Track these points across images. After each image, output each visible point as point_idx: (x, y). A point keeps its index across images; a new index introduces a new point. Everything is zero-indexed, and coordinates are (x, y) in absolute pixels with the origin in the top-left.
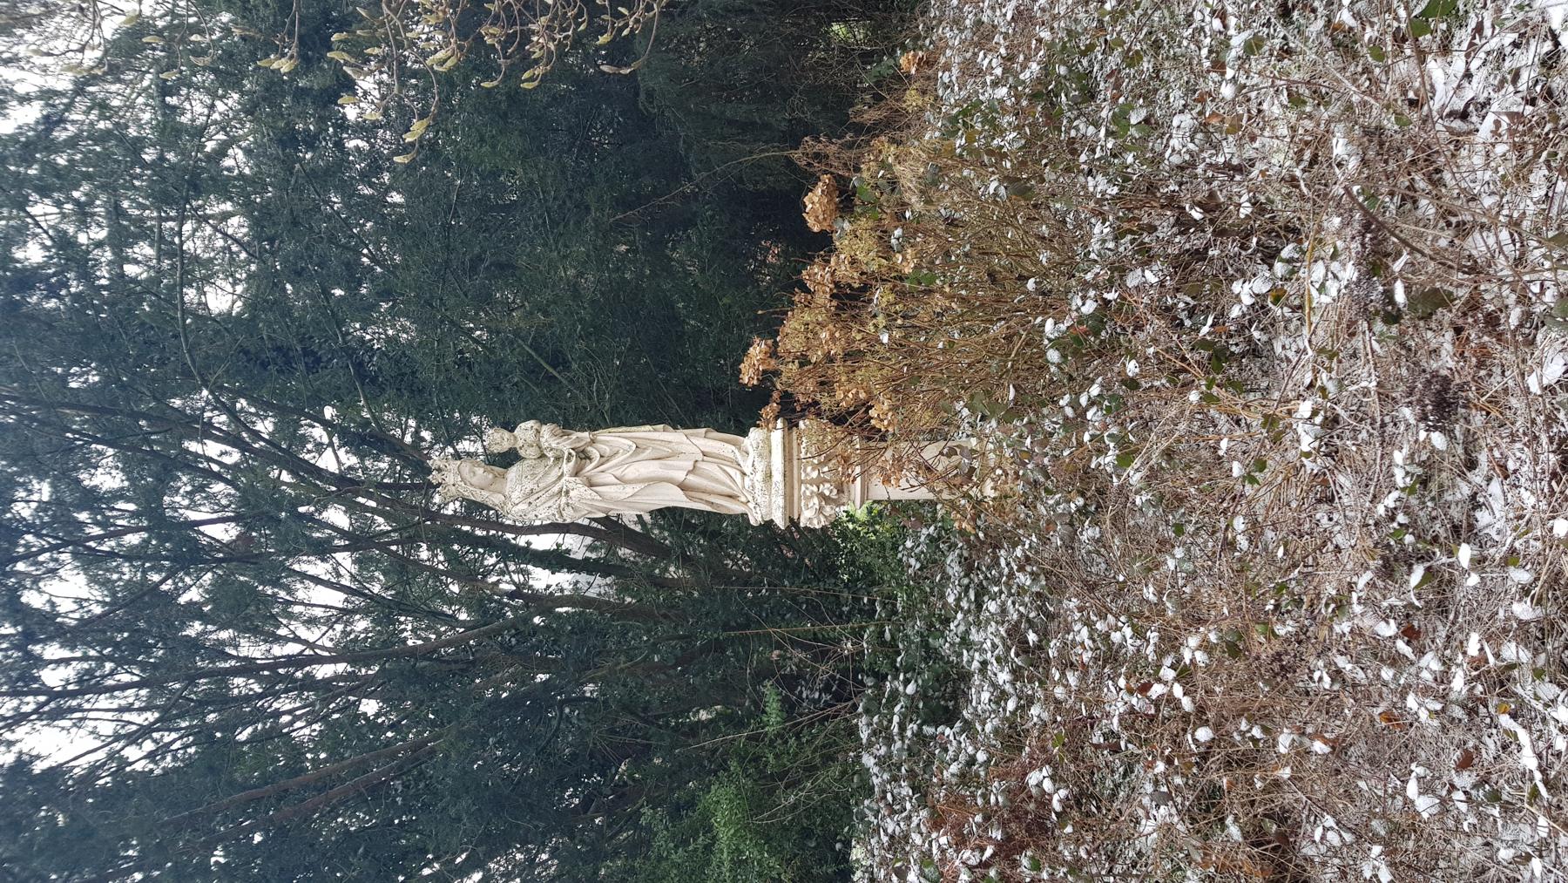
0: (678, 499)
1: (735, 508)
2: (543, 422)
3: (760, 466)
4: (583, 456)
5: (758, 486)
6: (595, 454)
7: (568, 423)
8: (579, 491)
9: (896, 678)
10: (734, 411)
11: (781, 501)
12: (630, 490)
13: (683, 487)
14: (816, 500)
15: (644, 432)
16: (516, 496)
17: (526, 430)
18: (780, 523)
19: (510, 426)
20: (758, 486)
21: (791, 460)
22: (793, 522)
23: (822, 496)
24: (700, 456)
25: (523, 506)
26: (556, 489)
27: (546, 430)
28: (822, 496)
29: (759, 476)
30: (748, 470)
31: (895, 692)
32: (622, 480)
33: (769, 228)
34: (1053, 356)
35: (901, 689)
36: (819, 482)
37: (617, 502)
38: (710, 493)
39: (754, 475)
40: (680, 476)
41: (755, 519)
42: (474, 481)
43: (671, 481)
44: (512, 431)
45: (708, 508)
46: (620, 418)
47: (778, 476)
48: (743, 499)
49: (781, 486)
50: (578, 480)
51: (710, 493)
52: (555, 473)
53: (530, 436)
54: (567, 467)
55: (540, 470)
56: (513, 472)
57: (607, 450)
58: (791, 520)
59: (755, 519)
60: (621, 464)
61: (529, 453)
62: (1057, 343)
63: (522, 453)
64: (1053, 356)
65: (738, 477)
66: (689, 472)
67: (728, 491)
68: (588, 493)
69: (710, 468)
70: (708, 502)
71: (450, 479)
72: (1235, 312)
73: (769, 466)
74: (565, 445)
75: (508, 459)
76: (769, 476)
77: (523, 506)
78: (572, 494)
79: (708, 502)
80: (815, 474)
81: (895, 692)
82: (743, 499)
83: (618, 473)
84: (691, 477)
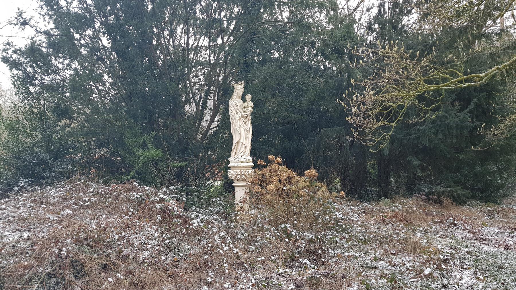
0: (235, 141)
1: (233, 154)
2: (253, 108)
3: (244, 160)
4: (246, 118)
5: (239, 160)
6: (246, 120)
7: (252, 114)
8: (238, 117)
10: (257, 153)
11: (236, 165)
12: (238, 129)
13: (239, 141)
15: (251, 132)
16: (236, 102)
17: (251, 104)
18: (229, 165)
19: (252, 100)
20: (239, 160)
22: (229, 168)
23: (237, 175)
27: (251, 109)
28: (237, 175)
29: (242, 160)
30: (243, 157)
31: (182, 195)
33: (295, 162)
34: (283, 226)
36: (241, 175)
37: (235, 125)
39: (241, 159)
40: (241, 141)
43: (240, 139)
45: (233, 148)
47: (242, 164)
52: (241, 111)
53: (250, 105)
54: (243, 114)
55: (242, 107)
56: (241, 101)
57: (247, 123)
61: (246, 105)
62: (285, 226)
63: (246, 103)
64: (283, 226)
65: (241, 155)
68: (237, 119)
71: (239, 86)
72: (301, 260)
74: (248, 113)
75: (243, 99)
81: (182, 195)
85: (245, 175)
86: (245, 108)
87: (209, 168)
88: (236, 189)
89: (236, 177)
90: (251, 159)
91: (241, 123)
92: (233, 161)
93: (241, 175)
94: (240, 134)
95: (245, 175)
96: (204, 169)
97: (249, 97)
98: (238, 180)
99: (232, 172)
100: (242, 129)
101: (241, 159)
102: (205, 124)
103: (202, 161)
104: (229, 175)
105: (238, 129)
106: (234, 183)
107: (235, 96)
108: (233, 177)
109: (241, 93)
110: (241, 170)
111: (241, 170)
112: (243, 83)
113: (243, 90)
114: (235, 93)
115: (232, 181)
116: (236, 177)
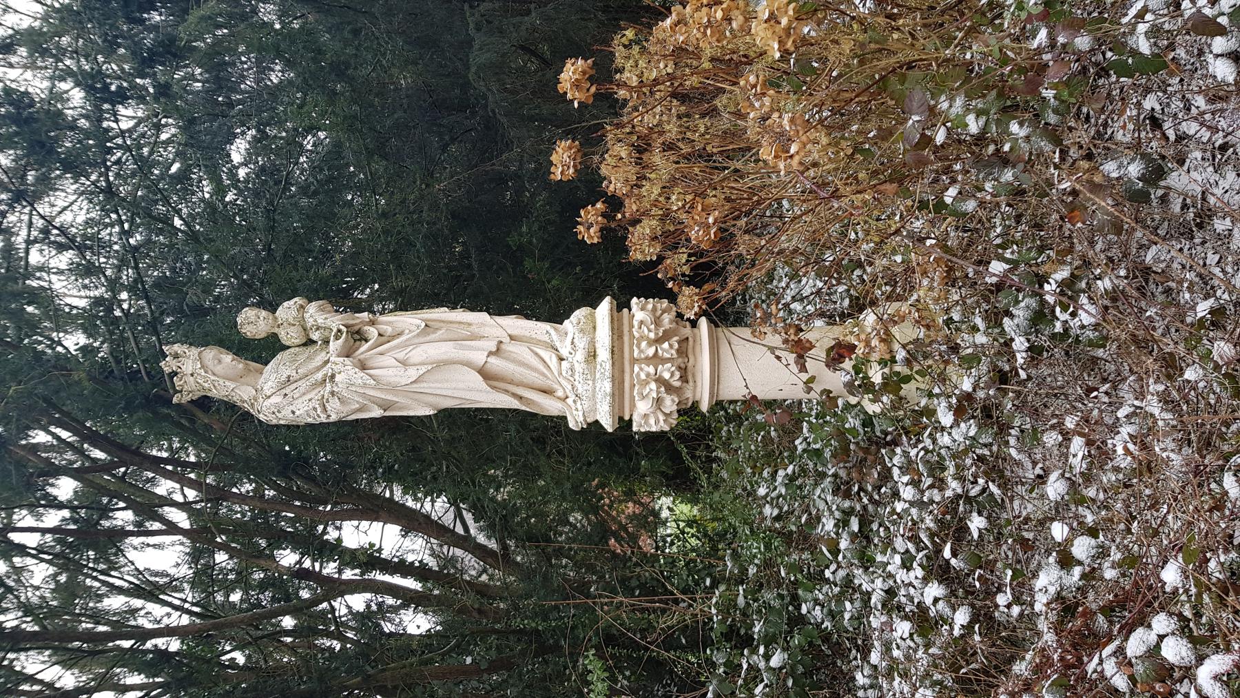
1: (549, 406)
3: (582, 343)
5: (579, 368)
6: (372, 332)
8: (347, 373)
9: (754, 651)
11: (607, 386)
13: (487, 375)
14: (653, 386)
15: (441, 314)
18: (608, 425)
20: (579, 368)
21: (621, 337)
23: (660, 381)
24: (506, 340)
25: (276, 399)
26: (319, 376)
27: (312, 308)
28: (660, 381)
29: (580, 356)
30: (564, 352)
32: (404, 363)
35: (762, 665)
36: (656, 359)
37: (393, 389)
38: (511, 382)
39: (578, 366)
40: (479, 358)
41: (576, 421)
42: (218, 369)
43: (468, 364)
44: (274, 311)
45: (515, 404)
46: (409, 301)
47: (604, 355)
48: (560, 393)
49: (608, 366)
50: (347, 361)
51: (511, 382)
57: (389, 330)
58: (621, 419)
59: (576, 421)
60: (404, 345)
65: (553, 361)
66: (490, 354)
67: (540, 381)
68: (359, 377)
69: (520, 351)
70: (514, 395)
71: (188, 366)
73: (592, 343)
75: (263, 350)
76: (592, 355)
77: (276, 399)
78: (338, 378)
79: (520, 398)
80: (651, 352)
82: (560, 393)
83: (401, 356)
84: (492, 360)
85: (659, 341)
86: (310, 342)
87: (619, 540)
88: (733, 389)
89: (670, 389)
90: (580, 313)
91: (388, 360)
92: (585, 401)
93: (656, 359)
94: (441, 364)
95: (659, 341)
96: (625, 559)
97: (253, 321)
98: (684, 379)
99: (643, 407)
100: (418, 354)
101: (578, 366)
102: (175, 645)
103: (591, 569)
104: (656, 424)
105: (413, 373)
106: (695, 405)
107: (242, 394)
108: (670, 404)
109: (228, 358)
110: (634, 361)
111: (634, 361)
112: (610, 430)
113: (210, 353)
114: (221, 389)
115: (689, 411)
116: (670, 389)
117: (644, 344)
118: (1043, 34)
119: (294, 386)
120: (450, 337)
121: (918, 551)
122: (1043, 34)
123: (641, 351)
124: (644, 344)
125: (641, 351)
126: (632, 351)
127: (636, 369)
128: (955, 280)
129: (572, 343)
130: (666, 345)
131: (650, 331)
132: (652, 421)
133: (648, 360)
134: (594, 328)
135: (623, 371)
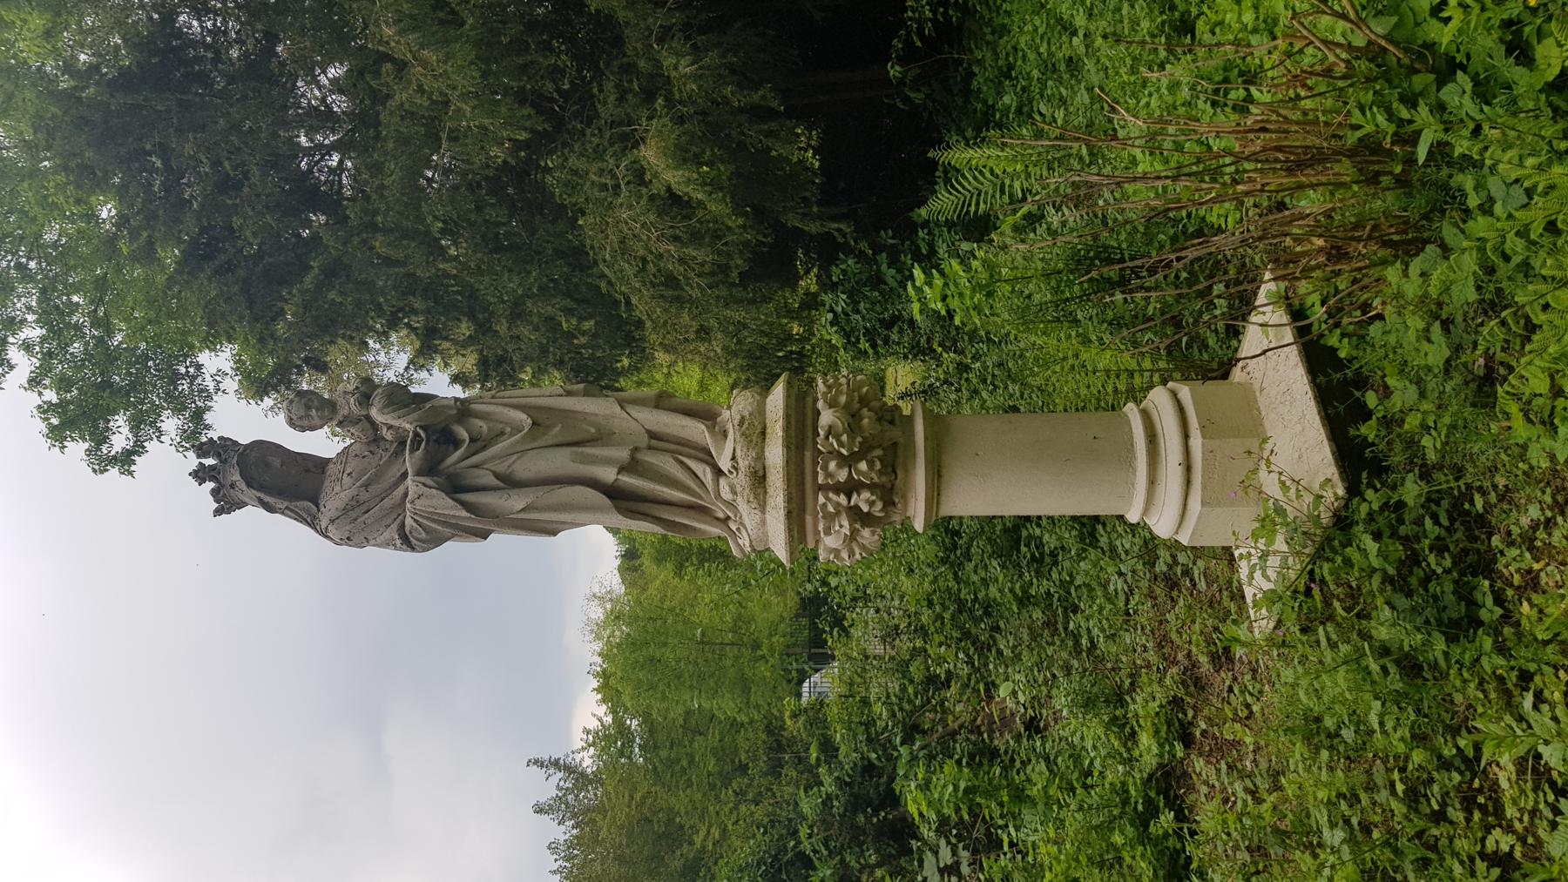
30: (725, 464)
73: (760, 457)
76: (759, 479)
83: (501, 468)
117: (832, 465)
118: (336, 158)
119: (364, 508)
120: (570, 439)
121: (1270, 792)
122: (336, 158)
123: (829, 475)
124: (832, 465)
125: (829, 475)
126: (815, 474)
127: (821, 499)
128: (687, 151)
129: (733, 458)
130: (863, 466)
131: (841, 444)
132: (845, 555)
133: (838, 488)
134: (763, 433)
135: (803, 484)
